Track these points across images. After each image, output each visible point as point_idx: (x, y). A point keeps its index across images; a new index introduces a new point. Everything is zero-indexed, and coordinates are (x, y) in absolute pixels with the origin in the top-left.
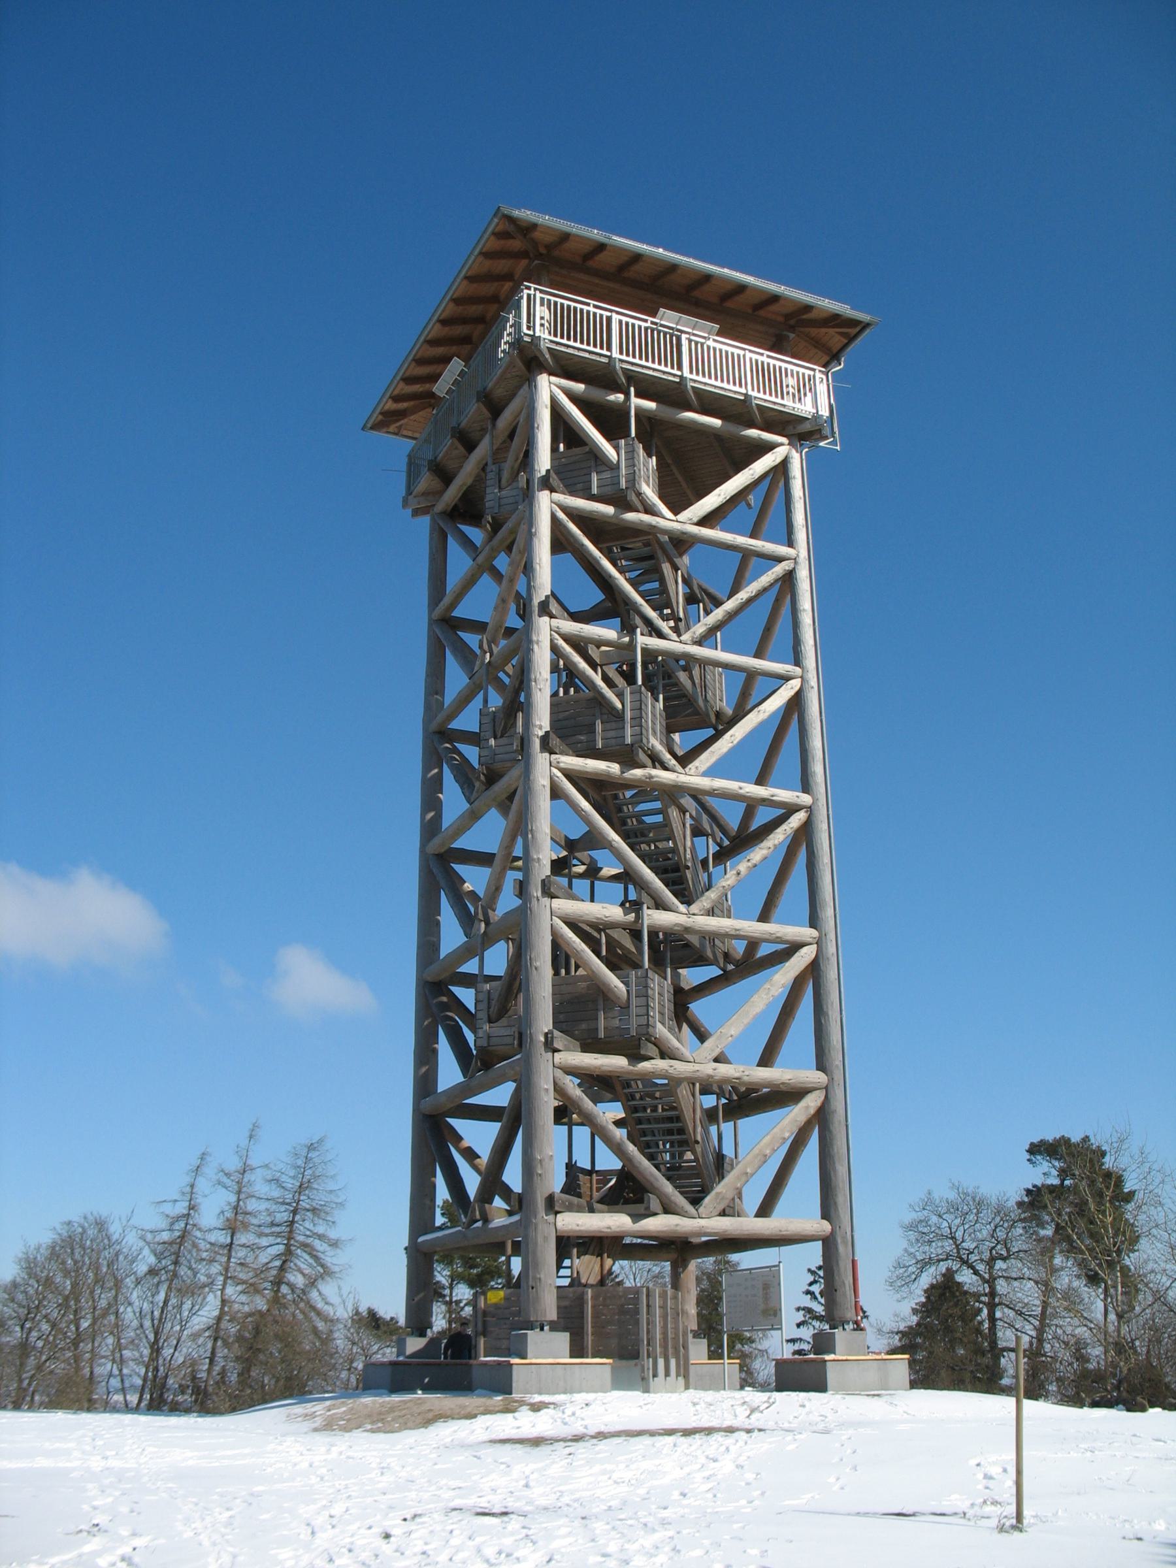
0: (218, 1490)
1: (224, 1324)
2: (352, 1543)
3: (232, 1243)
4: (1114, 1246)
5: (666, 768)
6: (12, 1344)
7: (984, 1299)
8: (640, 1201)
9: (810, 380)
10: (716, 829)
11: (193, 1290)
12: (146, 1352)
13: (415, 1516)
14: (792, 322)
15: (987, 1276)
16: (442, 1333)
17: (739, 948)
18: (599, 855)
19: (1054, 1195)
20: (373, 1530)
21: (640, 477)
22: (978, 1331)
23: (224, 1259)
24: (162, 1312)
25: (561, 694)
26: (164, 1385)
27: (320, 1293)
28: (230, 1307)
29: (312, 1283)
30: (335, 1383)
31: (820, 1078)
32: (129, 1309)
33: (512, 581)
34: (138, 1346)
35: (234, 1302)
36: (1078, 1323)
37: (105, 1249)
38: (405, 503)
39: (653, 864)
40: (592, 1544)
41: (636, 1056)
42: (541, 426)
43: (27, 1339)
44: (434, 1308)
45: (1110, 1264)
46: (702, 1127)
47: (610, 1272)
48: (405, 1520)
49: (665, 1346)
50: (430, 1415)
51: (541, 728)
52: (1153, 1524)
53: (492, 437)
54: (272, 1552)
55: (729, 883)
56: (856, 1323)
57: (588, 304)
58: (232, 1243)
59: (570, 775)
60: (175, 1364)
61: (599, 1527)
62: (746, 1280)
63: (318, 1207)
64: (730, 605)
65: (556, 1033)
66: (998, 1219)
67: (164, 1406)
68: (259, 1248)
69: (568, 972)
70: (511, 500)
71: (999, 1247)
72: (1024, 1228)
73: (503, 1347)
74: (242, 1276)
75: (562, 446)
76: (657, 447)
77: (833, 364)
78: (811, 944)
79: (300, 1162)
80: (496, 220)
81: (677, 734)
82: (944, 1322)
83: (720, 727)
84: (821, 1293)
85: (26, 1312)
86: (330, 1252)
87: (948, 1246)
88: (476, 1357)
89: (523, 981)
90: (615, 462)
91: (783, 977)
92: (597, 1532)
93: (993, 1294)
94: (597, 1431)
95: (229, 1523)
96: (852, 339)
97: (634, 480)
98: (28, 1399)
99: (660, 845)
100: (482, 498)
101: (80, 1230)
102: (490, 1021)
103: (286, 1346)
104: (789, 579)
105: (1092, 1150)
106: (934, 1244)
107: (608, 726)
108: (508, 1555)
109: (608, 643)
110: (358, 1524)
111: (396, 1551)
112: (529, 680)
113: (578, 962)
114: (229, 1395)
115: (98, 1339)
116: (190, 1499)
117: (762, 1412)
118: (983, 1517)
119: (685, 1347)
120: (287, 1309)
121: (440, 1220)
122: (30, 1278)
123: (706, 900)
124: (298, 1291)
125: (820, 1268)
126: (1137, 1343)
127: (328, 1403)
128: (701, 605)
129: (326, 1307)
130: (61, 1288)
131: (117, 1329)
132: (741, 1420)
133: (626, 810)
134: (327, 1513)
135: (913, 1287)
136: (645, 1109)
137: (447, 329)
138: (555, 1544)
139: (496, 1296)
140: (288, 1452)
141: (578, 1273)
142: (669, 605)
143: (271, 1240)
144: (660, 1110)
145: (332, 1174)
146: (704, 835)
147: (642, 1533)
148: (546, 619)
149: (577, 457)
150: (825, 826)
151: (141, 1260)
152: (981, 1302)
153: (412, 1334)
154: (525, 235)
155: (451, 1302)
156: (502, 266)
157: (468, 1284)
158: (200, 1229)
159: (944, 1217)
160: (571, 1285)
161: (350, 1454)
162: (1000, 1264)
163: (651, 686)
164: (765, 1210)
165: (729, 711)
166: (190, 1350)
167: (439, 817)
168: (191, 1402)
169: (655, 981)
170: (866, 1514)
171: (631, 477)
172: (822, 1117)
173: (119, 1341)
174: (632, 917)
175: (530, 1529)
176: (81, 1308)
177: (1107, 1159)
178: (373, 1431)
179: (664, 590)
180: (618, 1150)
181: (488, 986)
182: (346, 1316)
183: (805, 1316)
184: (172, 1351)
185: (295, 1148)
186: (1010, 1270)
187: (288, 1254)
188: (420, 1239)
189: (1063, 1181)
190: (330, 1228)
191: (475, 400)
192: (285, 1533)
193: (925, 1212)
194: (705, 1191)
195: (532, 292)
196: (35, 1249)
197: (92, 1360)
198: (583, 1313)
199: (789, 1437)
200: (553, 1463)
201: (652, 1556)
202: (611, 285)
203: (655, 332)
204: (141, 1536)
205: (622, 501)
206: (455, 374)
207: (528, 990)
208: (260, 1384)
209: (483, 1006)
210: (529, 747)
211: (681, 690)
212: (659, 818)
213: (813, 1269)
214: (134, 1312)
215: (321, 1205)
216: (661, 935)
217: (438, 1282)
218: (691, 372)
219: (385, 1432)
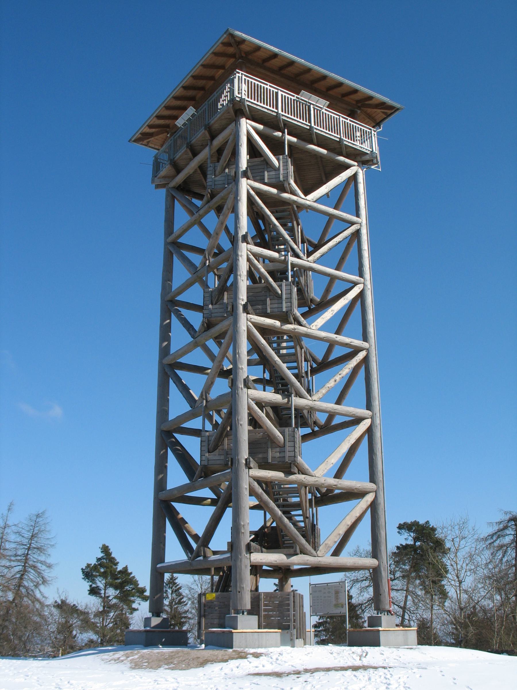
5: (301, 325)
14: (359, 105)
27: (40, 592)
38: (153, 181)
51: (243, 300)
53: (210, 147)
57: (267, 85)
70: (221, 182)
80: (225, 36)
86: (48, 570)
90: (277, 167)
96: (389, 116)
97: (287, 176)
102: (209, 452)
104: (357, 234)
107: (273, 301)
154: (237, 46)
157: (114, 588)
164: (336, 553)
171: (286, 175)
174: (286, 400)
185: (30, 516)
187: (23, 573)
188: (159, 566)
190: (47, 557)
202: (275, 76)
205: (282, 187)
206: (189, 116)
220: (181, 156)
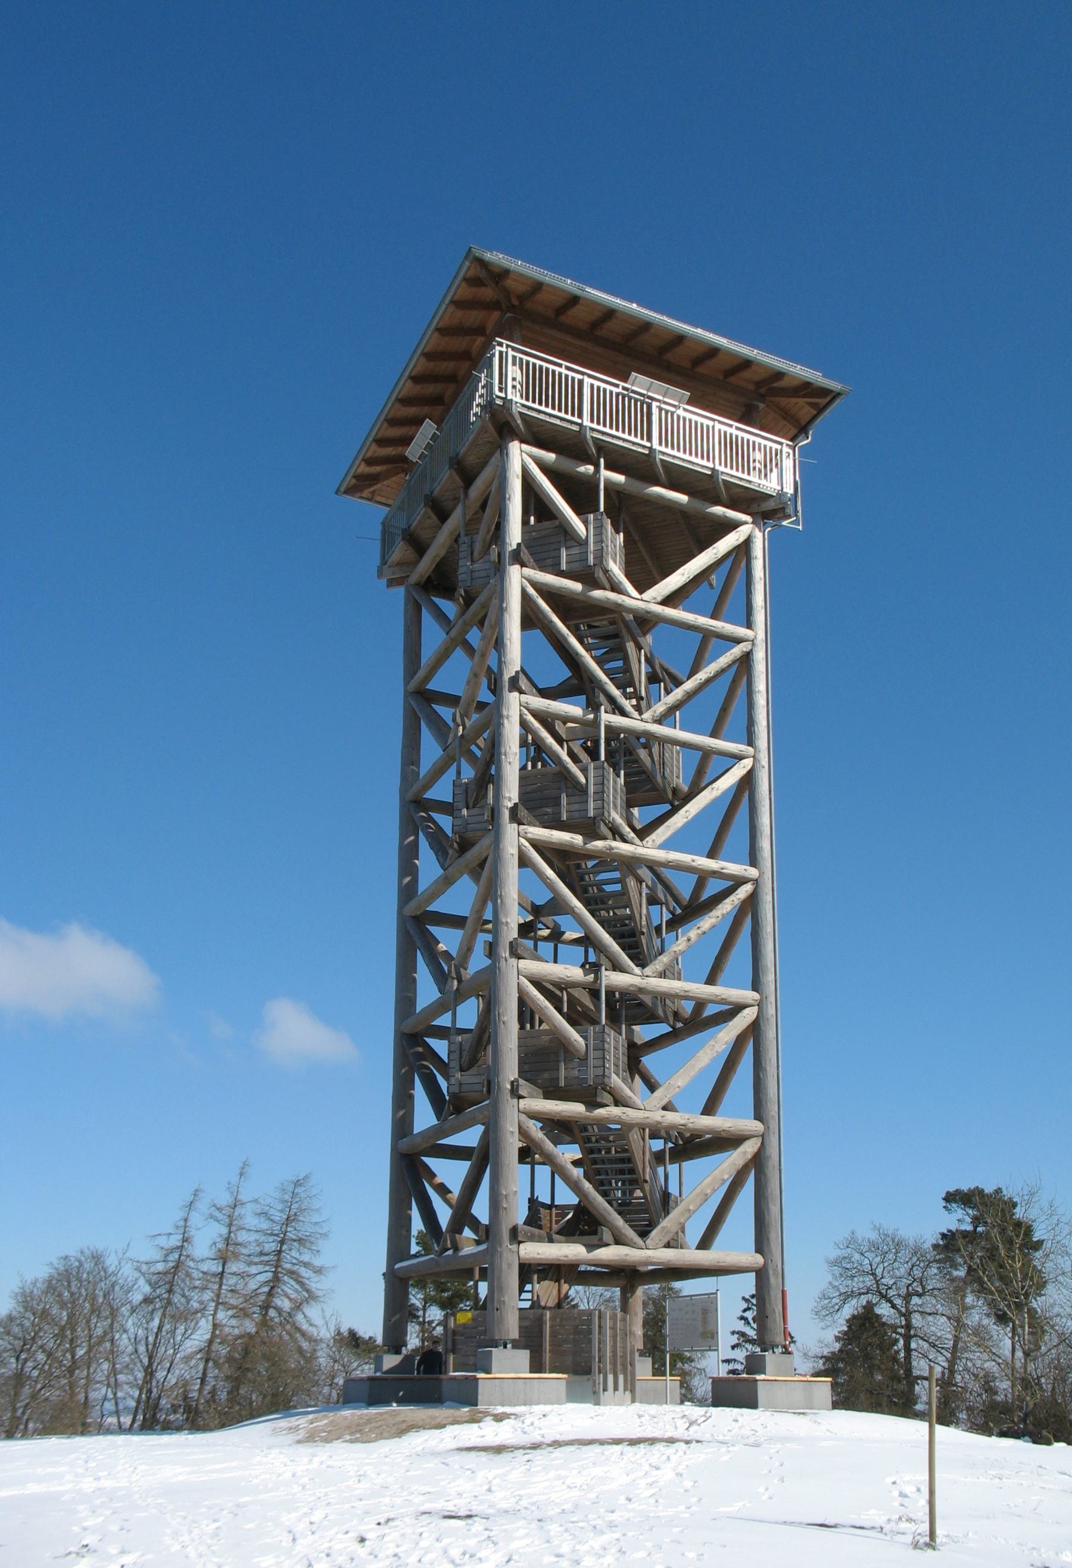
0: (206, 1503)
1: (215, 1346)
2: (330, 1548)
3: (223, 1272)
4: (1022, 1289)
5: (625, 841)
6: (6, 1375)
7: (899, 1330)
8: (594, 1232)
9: (776, 455)
10: (670, 898)
11: (187, 1316)
12: (140, 1375)
13: (388, 1520)
14: (763, 391)
15: (903, 1310)
16: (416, 1351)
17: (688, 1008)
18: (562, 920)
19: (967, 1240)
20: (350, 1535)
21: (607, 554)
22: (895, 1359)
23: (216, 1286)
24: (156, 1337)
25: (529, 767)
26: (157, 1405)
27: (305, 1316)
28: (221, 1331)
29: (298, 1307)
30: (317, 1398)
31: (757, 1126)
32: (125, 1336)
33: (483, 655)
34: (132, 1370)
35: (225, 1325)
36: (987, 1358)
37: (101, 1280)
38: (380, 574)
39: (611, 929)
40: (547, 1545)
41: (593, 1104)
42: (512, 497)
43: (22, 1369)
44: (409, 1328)
45: (1019, 1306)
46: (651, 1168)
47: (567, 1296)
48: (379, 1524)
49: (614, 1363)
50: (404, 1426)
51: (510, 799)
52: (1060, 1555)
54: (255, 1560)
55: (680, 948)
56: (785, 1347)
57: (560, 365)
58: (223, 1272)
59: (536, 845)
60: (167, 1385)
61: (554, 1528)
62: (687, 1305)
63: (304, 1237)
64: (689, 685)
65: (522, 1082)
66: (915, 1259)
67: (157, 1425)
68: (249, 1276)
69: (532, 1027)
71: (915, 1284)
72: (939, 1268)
73: (471, 1363)
74: (233, 1302)
75: (532, 518)
76: (624, 523)
77: (801, 438)
78: (753, 1006)
79: (287, 1197)
80: (467, 264)
81: (636, 809)
82: (863, 1349)
83: (677, 803)
84: (754, 1319)
85: (22, 1344)
86: (314, 1278)
87: (869, 1281)
88: (446, 1372)
89: (492, 1034)
90: (584, 538)
91: (726, 1034)
92: (552, 1533)
93: (908, 1326)
94: (553, 1439)
95: (215, 1534)
96: (821, 410)
97: (602, 556)
98: (22, 1427)
99: (618, 912)
100: (455, 570)
101: (77, 1264)
102: (462, 1070)
103: (273, 1365)
104: (746, 659)
105: (1004, 1201)
106: (856, 1279)
107: (573, 799)
108: (471, 1556)
109: (574, 720)
110: (335, 1530)
111: (371, 1554)
112: (500, 754)
113: (542, 1017)
114: (219, 1413)
115: (94, 1366)
116: (179, 1514)
117: (699, 1425)
118: (898, 1533)
119: (632, 1364)
120: (274, 1330)
121: (415, 1249)
122: (26, 1311)
123: (658, 965)
124: (285, 1315)
125: (753, 1296)
126: (1043, 1380)
127: (311, 1416)
128: (662, 684)
129: (311, 1329)
130: (57, 1319)
131: (112, 1355)
132: (680, 1432)
133: (587, 879)
134: (307, 1520)
135: (836, 1317)
136: (600, 1151)
137: (419, 387)
138: (514, 1545)
139: (465, 1316)
140: (272, 1464)
141: (538, 1296)
142: (631, 684)
143: (260, 1268)
144: (613, 1152)
145: (317, 1207)
146: (658, 904)
147: (592, 1534)
148: (516, 694)
149: (547, 532)
150: (769, 898)
151: (136, 1290)
152: (898, 1333)
153: (388, 1352)
154: (497, 283)
155: (424, 1322)
156: (474, 317)
158: (193, 1260)
159: (866, 1255)
160: (532, 1307)
161: (330, 1463)
162: (915, 1300)
163: (613, 762)
164: (705, 1243)
165: (685, 788)
166: (183, 1372)
167: (415, 881)
168: (183, 1420)
169: (611, 1036)
170: (792, 1523)
172: (758, 1162)
173: (114, 1366)
174: (591, 977)
175: (491, 1530)
176: (77, 1337)
177: (1017, 1210)
178: (351, 1441)
179: (627, 669)
180: (575, 1187)
181: (459, 1038)
182: (328, 1336)
183: (739, 1339)
184: (165, 1373)
186: (925, 1306)
188: (397, 1266)
189: (975, 1228)
190: (315, 1256)
191: (447, 467)
192: (268, 1541)
193: (849, 1250)
194: (652, 1225)
195: (504, 349)
196: (31, 1283)
197: (87, 1386)
198: (542, 1332)
199: (724, 1449)
200: (514, 1469)
201: (600, 1556)
202: (583, 344)
203: (626, 399)
204: (129, 1552)
205: (589, 577)
207: (496, 1042)
208: (248, 1400)
209: (456, 1056)
210: (499, 817)
211: (641, 767)
212: (618, 887)
213: (747, 1297)
214: (130, 1340)
215: (306, 1236)
216: (617, 994)
217: (413, 1304)
218: (660, 444)
219: (363, 1442)
220: (420, 522)
